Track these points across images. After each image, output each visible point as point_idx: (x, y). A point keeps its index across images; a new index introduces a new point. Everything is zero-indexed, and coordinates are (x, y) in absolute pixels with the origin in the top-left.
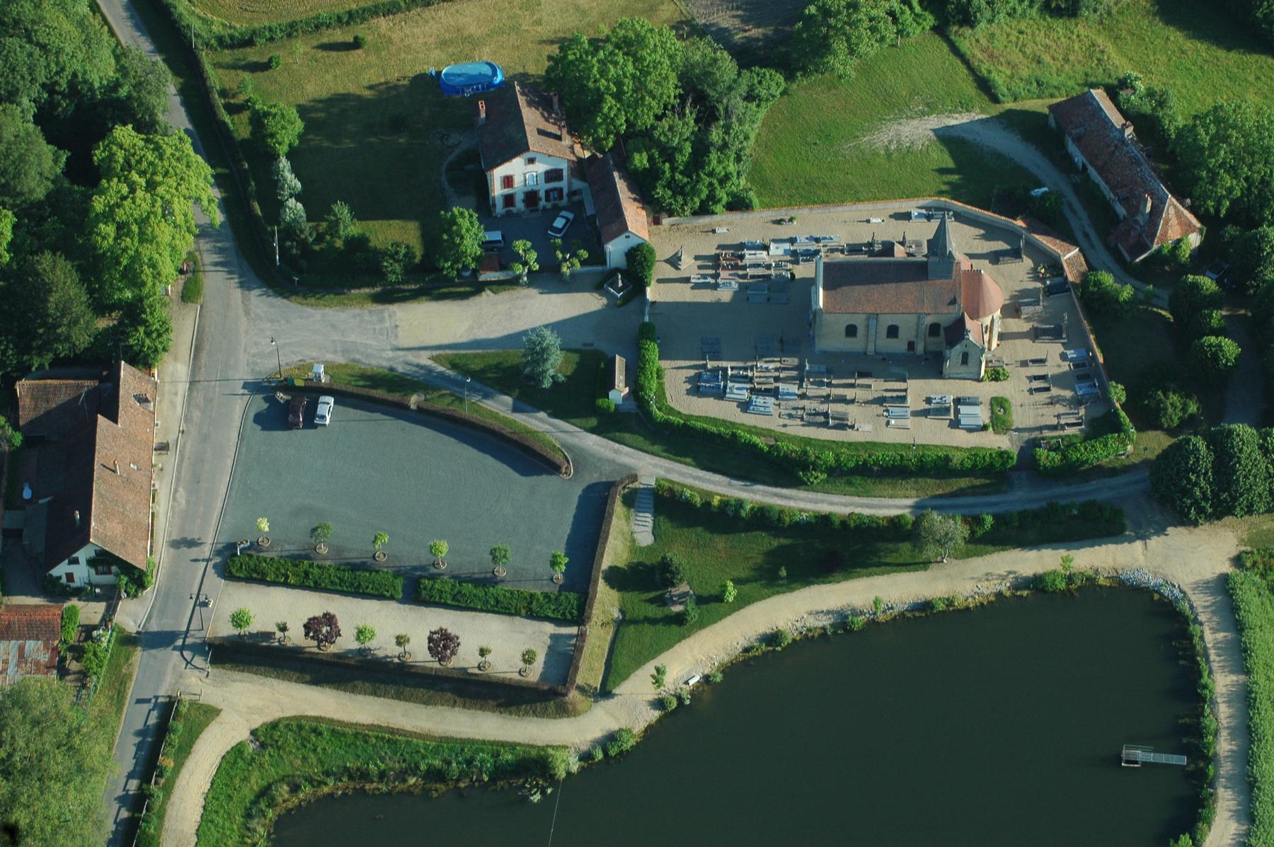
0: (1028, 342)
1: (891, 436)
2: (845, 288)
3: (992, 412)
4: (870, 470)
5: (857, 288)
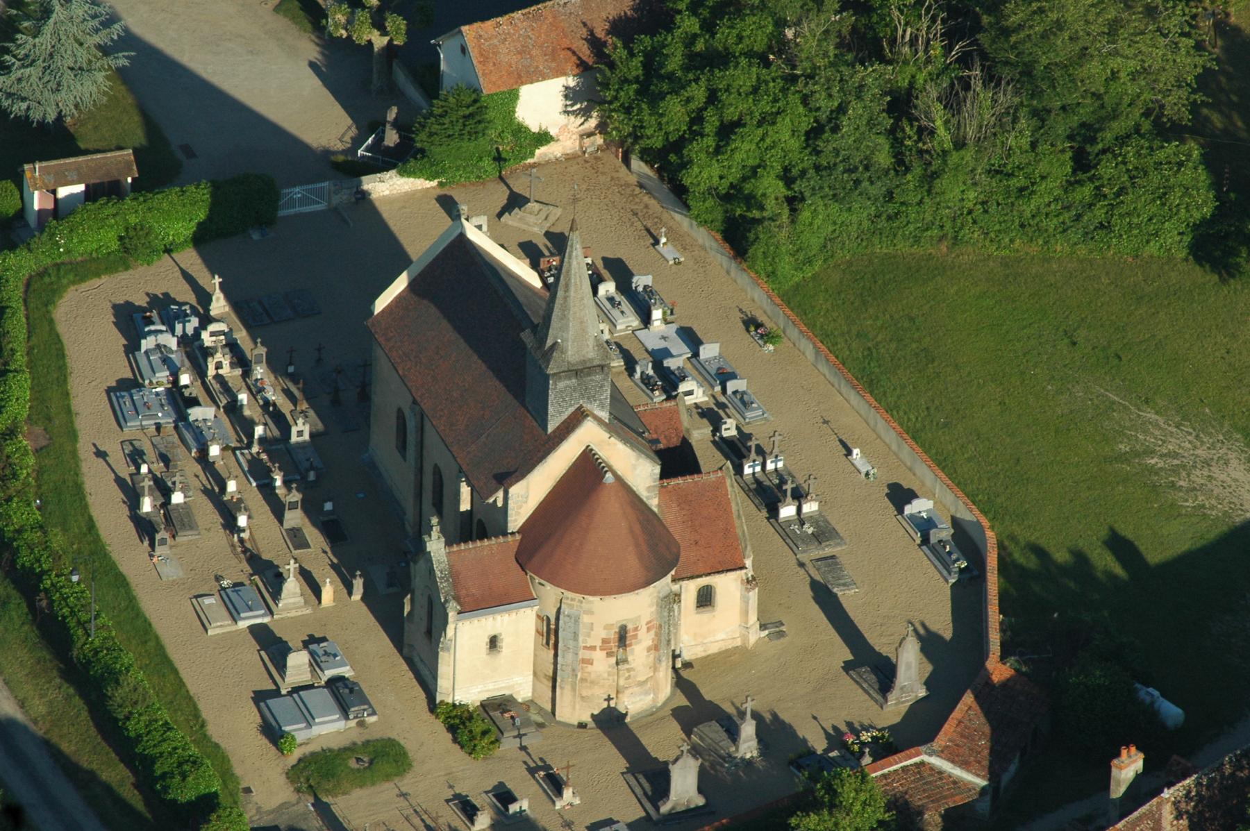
0: (622, 764)
1: (166, 615)
2: (433, 310)
3: (346, 749)
4: (36, 590)
5: (445, 324)
